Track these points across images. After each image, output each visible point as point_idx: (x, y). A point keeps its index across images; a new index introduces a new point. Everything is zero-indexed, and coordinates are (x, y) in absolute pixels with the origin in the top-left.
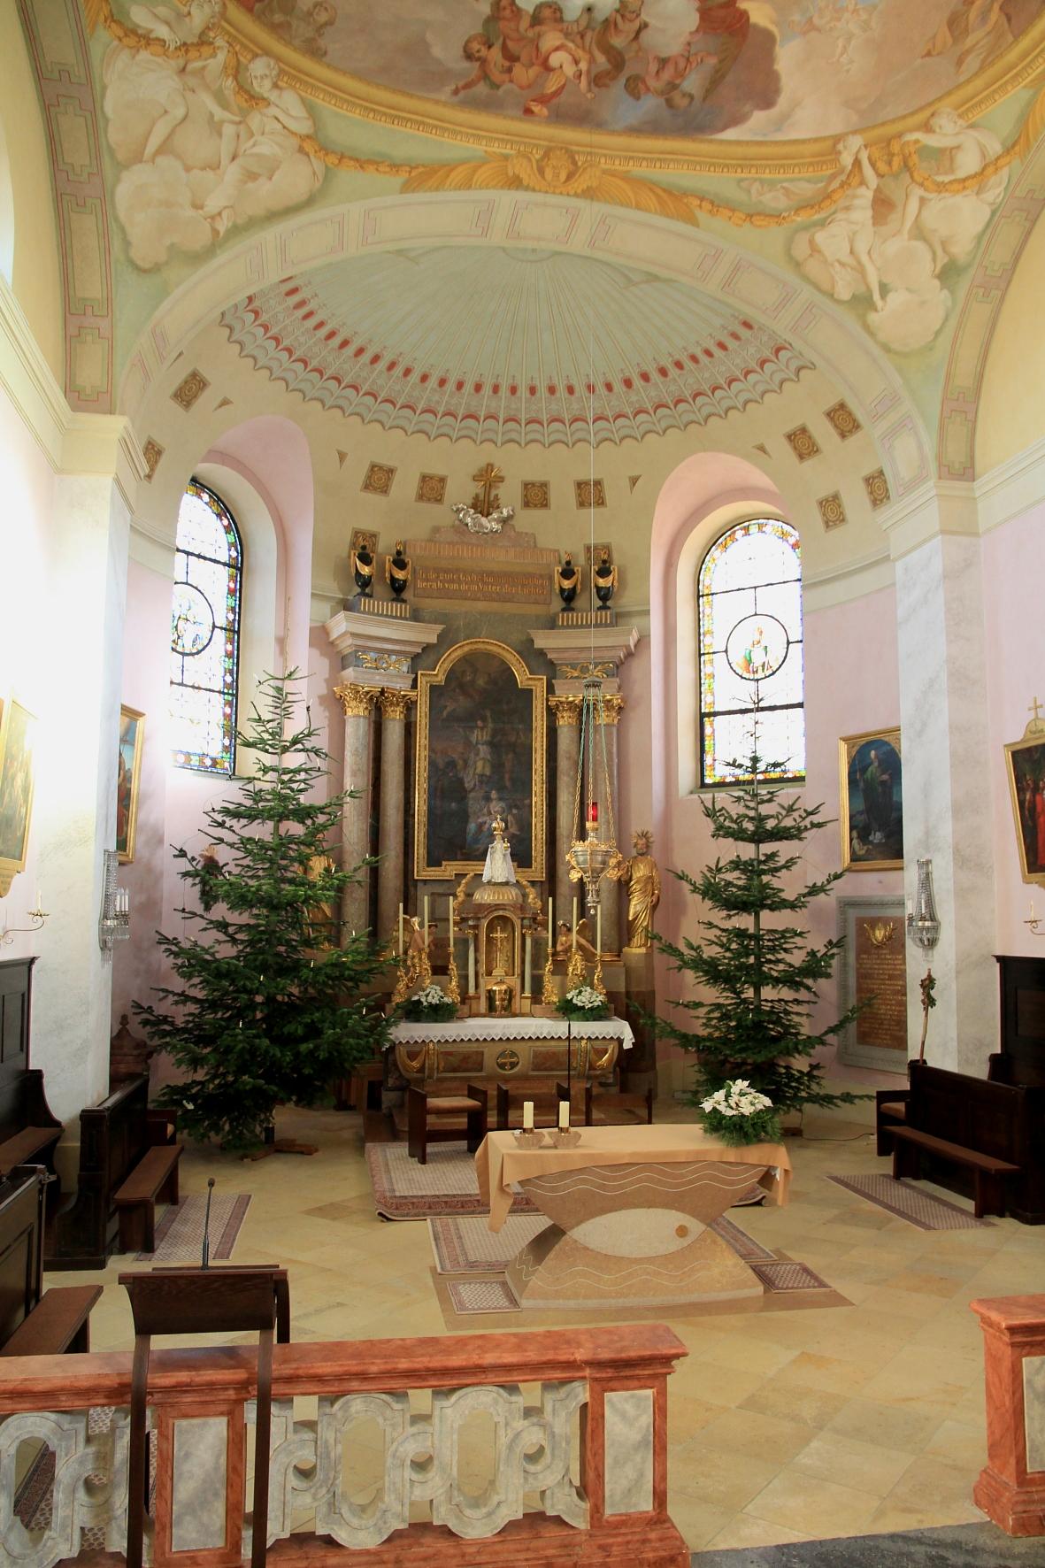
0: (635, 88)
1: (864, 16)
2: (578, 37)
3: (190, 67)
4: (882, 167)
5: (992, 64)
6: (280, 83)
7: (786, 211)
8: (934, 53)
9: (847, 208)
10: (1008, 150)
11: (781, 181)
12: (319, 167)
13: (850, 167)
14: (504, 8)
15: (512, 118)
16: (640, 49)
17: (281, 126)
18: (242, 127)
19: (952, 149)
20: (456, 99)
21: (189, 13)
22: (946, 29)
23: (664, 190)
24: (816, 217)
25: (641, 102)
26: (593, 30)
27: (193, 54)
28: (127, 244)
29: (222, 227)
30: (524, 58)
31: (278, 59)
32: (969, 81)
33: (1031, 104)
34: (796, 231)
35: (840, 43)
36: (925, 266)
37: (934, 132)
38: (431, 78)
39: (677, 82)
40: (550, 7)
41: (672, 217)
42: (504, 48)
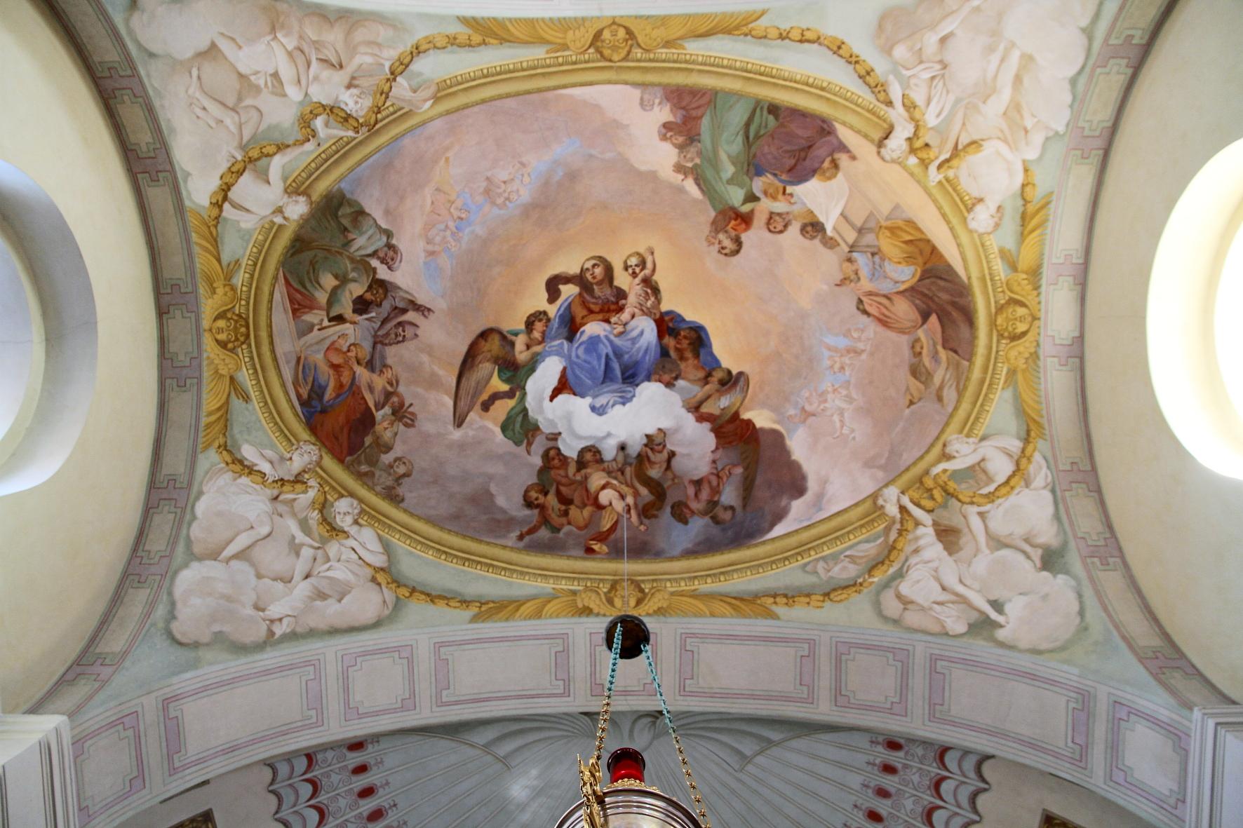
0: (681, 514)
1: (844, 392)
2: (619, 473)
3: (282, 497)
4: (928, 504)
5: (965, 387)
6: (360, 521)
7: (859, 577)
8: (915, 401)
9: (916, 551)
10: (1027, 440)
11: (842, 552)
12: (389, 596)
13: (899, 516)
14: (553, 459)
15: (576, 558)
16: (675, 477)
17: (356, 557)
18: (320, 552)
19: (979, 463)
20: (521, 544)
21: (291, 459)
22: (913, 379)
23: (735, 598)
24: (891, 571)
25: (690, 525)
26: (630, 465)
27: (287, 488)
28: (172, 616)
29: (279, 630)
30: (577, 500)
31: (361, 501)
32: (956, 409)
33: (1017, 398)
34: (878, 593)
35: (836, 418)
36: (1024, 569)
37: (954, 457)
38: (498, 525)
39: (716, 499)
40: (590, 451)
41: (750, 617)
42: (558, 493)
